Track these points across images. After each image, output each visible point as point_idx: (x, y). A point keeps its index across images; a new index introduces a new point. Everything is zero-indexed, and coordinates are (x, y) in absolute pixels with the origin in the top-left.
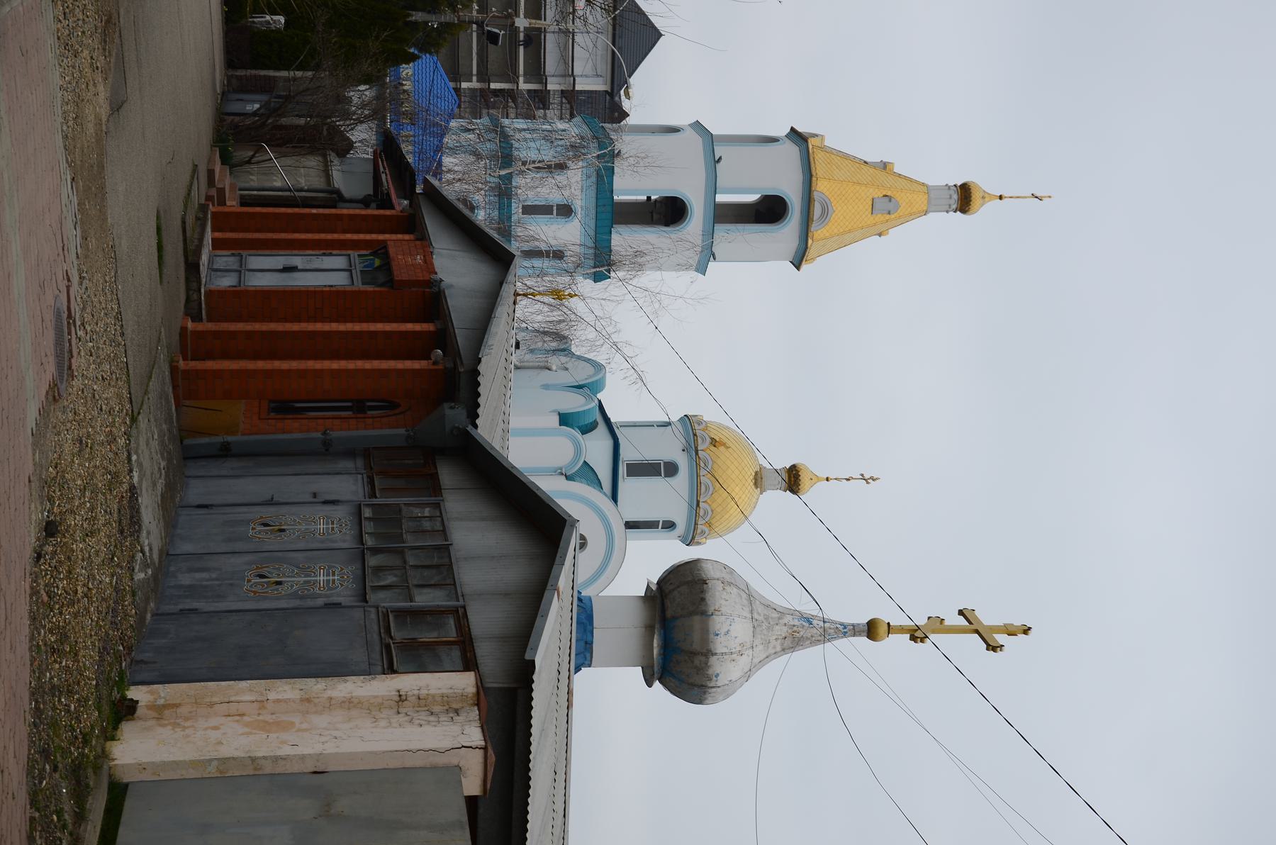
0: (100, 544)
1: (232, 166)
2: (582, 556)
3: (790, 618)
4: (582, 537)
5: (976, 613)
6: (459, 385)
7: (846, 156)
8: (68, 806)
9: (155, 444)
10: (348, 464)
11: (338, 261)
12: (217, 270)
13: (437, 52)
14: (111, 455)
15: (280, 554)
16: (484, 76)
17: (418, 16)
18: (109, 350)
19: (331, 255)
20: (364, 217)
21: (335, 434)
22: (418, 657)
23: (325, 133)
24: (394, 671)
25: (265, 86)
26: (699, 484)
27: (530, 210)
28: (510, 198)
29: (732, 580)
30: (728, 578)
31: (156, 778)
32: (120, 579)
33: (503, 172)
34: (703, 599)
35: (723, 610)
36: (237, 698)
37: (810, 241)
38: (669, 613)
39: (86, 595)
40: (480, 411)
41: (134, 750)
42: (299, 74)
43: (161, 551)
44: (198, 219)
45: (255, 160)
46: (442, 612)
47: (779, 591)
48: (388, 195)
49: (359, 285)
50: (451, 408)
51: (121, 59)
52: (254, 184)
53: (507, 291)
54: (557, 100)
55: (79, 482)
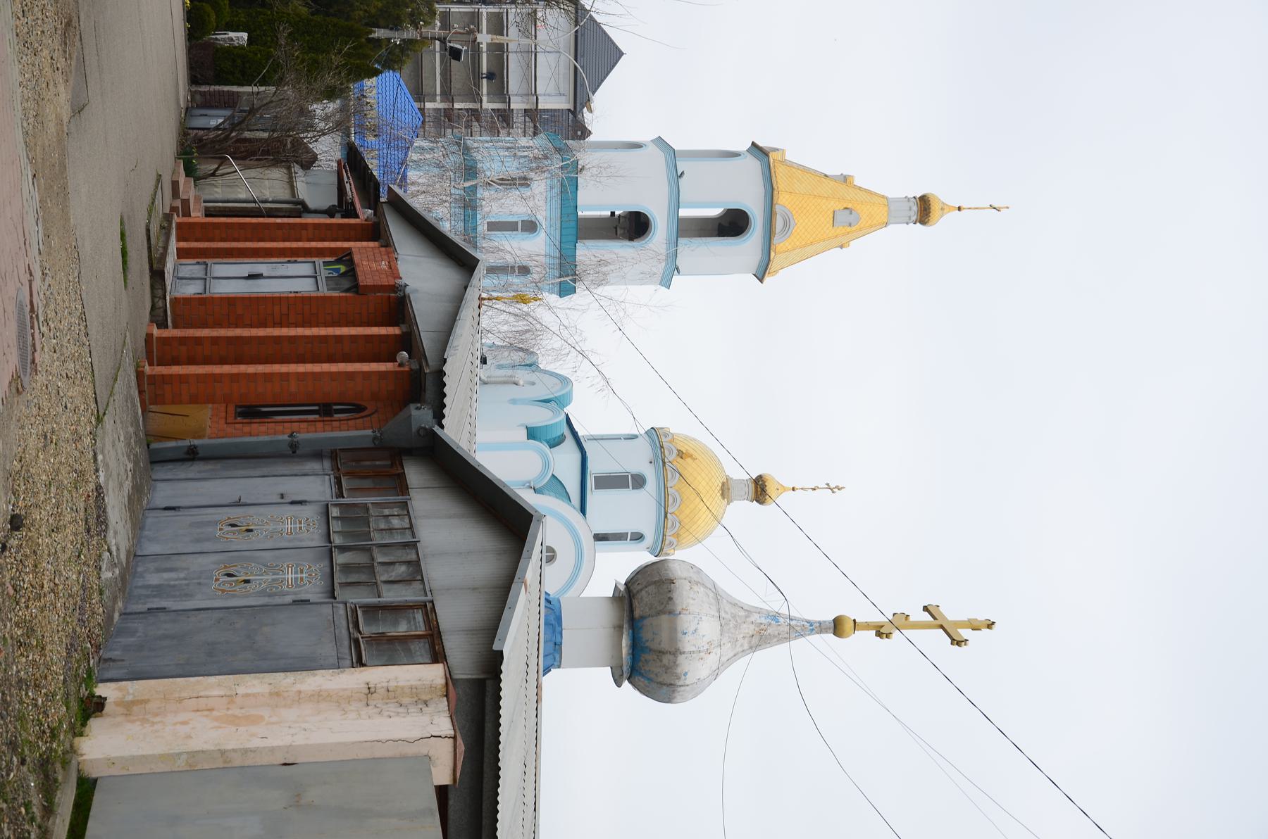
0: (67, 539)
1: (197, 179)
2: (549, 570)
3: (757, 616)
4: (550, 549)
5: (941, 609)
6: (425, 386)
8: (36, 800)
9: (121, 446)
10: (315, 466)
11: (304, 268)
12: (182, 278)
13: (400, 69)
14: (77, 454)
16: (447, 95)
17: (380, 33)
18: (73, 349)
19: (296, 262)
20: (328, 226)
21: (301, 436)
22: (391, 649)
23: (289, 145)
24: (363, 665)
25: (229, 101)
26: (666, 495)
27: (493, 226)
28: (474, 208)
29: (699, 579)
30: (695, 577)
31: (126, 773)
32: (86, 578)
33: (467, 184)
34: (670, 599)
35: (691, 608)
36: (207, 693)
37: (772, 254)
38: (637, 613)
39: (52, 591)
40: (446, 411)
41: (101, 746)
43: (128, 552)
44: (162, 228)
45: (218, 173)
46: (411, 607)
47: (748, 591)
48: (352, 204)
49: (324, 291)
50: (418, 408)
51: (82, 63)
52: (219, 197)
53: (472, 295)
54: (521, 119)
55: (44, 477)
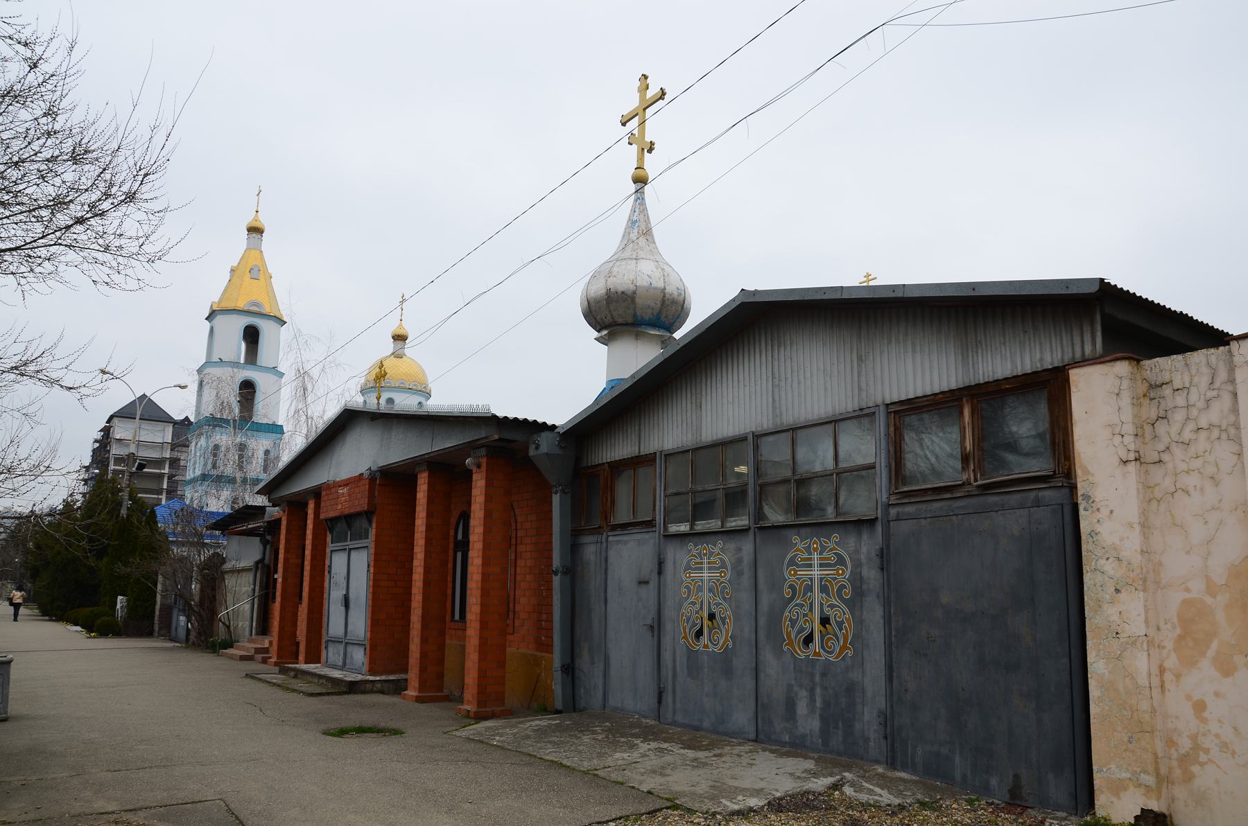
6: (505, 443)
7: (225, 291)
11: (338, 562)
15: (762, 621)
16: (159, 492)
17: (124, 512)
19: (330, 567)
25: (167, 611)
35: (632, 277)
38: (630, 320)
42: (159, 587)
44: (295, 677)
49: (370, 541)
52: (247, 623)
